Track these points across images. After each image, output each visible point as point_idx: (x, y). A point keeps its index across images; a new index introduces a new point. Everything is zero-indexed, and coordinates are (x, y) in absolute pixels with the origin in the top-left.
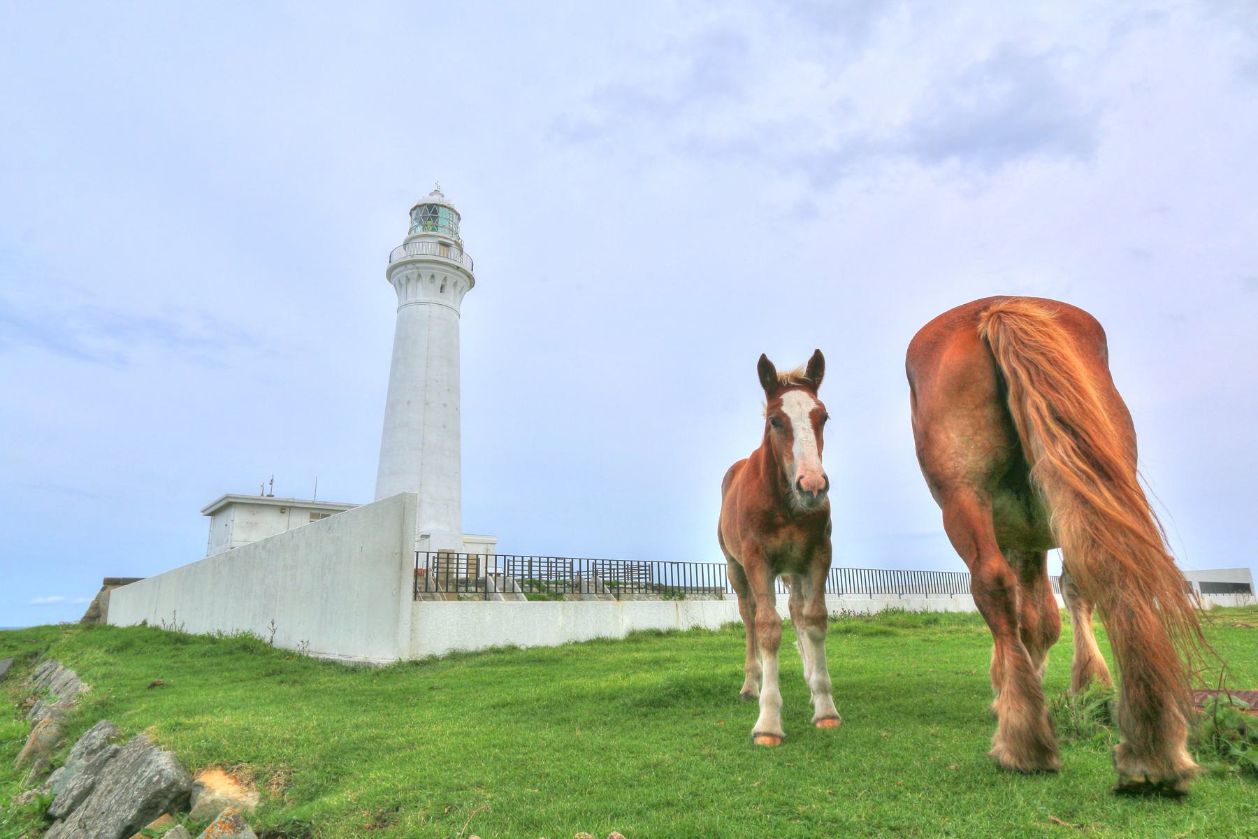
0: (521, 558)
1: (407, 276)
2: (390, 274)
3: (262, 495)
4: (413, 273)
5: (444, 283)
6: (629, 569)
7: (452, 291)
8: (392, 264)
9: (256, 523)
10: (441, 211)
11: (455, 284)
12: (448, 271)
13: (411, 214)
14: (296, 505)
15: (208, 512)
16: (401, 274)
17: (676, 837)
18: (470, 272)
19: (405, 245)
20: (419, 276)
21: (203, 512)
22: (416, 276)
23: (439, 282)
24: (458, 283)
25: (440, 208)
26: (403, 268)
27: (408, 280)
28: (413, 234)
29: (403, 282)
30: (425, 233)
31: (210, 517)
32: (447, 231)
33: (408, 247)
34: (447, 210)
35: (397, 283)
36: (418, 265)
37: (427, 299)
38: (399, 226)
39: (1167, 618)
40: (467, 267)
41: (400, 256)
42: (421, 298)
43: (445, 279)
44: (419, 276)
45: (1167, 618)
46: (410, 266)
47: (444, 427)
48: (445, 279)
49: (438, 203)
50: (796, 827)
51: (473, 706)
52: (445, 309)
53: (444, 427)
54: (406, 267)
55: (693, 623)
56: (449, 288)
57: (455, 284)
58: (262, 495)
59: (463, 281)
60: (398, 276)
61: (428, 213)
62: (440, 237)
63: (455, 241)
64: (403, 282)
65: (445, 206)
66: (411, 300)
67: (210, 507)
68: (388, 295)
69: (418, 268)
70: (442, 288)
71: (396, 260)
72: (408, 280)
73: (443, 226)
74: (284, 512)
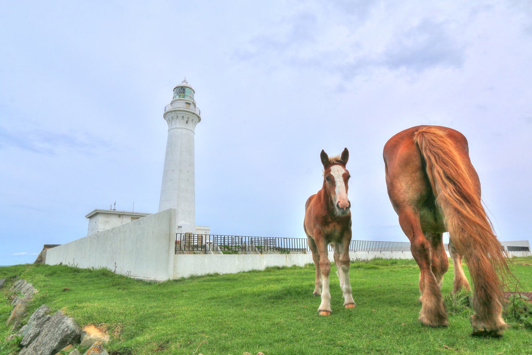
0: (220, 236)
1: (172, 117)
2: (165, 116)
3: (111, 209)
4: (175, 116)
5: (188, 120)
6: (266, 241)
7: (191, 123)
8: (166, 112)
9: (108, 221)
10: (187, 89)
11: (193, 120)
12: (189, 115)
13: (174, 90)
14: (125, 214)
15: (88, 216)
16: (170, 116)
17: (286, 354)
18: (199, 115)
19: (171, 104)
20: (177, 117)
21: (86, 217)
22: (176, 117)
23: (186, 120)
24: (194, 120)
25: (186, 88)
26: (170, 113)
27: (173, 118)
28: (175, 99)
29: (171, 119)
30: (180, 99)
31: (89, 219)
32: (189, 98)
33: (172, 104)
34: (189, 89)
35: (168, 120)
36: (177, 112)
37: (180, 127)
38: (169, 96)
39: (494, 261)
40: (197, 113)
41: (169, 108)
42: (178, 126)
43: (188, 118)
44: (177, 117)
45: (494, 261)
46: (173, 113)
47: (188, 181)
48: (188, 118)
49: (185, 86)
50: (337, 350)
51: (200, 299)
52: (188, 131)
53: (188, 181)
54: (172, 113)
55: (293, 264)
56: (190, 122)
57: (193, 120)
58: (111, 209)
59: (196, 119)
60: (168, 117)
61: (181, 90)
62: (186, 100)
63: (193, 102)
64: (171, 119)
65: (188, 87)
66: (174, 127)
67: (89, 215)
68: (164, 125)
69: (177, 113)
70: (187, 122)
71: (167, 110)
72: (173, 118)
73: (187, 96)
74: (120, 217)
